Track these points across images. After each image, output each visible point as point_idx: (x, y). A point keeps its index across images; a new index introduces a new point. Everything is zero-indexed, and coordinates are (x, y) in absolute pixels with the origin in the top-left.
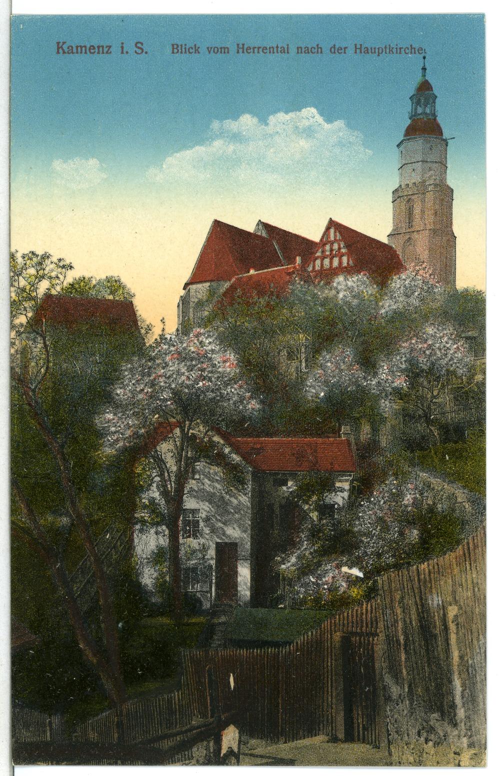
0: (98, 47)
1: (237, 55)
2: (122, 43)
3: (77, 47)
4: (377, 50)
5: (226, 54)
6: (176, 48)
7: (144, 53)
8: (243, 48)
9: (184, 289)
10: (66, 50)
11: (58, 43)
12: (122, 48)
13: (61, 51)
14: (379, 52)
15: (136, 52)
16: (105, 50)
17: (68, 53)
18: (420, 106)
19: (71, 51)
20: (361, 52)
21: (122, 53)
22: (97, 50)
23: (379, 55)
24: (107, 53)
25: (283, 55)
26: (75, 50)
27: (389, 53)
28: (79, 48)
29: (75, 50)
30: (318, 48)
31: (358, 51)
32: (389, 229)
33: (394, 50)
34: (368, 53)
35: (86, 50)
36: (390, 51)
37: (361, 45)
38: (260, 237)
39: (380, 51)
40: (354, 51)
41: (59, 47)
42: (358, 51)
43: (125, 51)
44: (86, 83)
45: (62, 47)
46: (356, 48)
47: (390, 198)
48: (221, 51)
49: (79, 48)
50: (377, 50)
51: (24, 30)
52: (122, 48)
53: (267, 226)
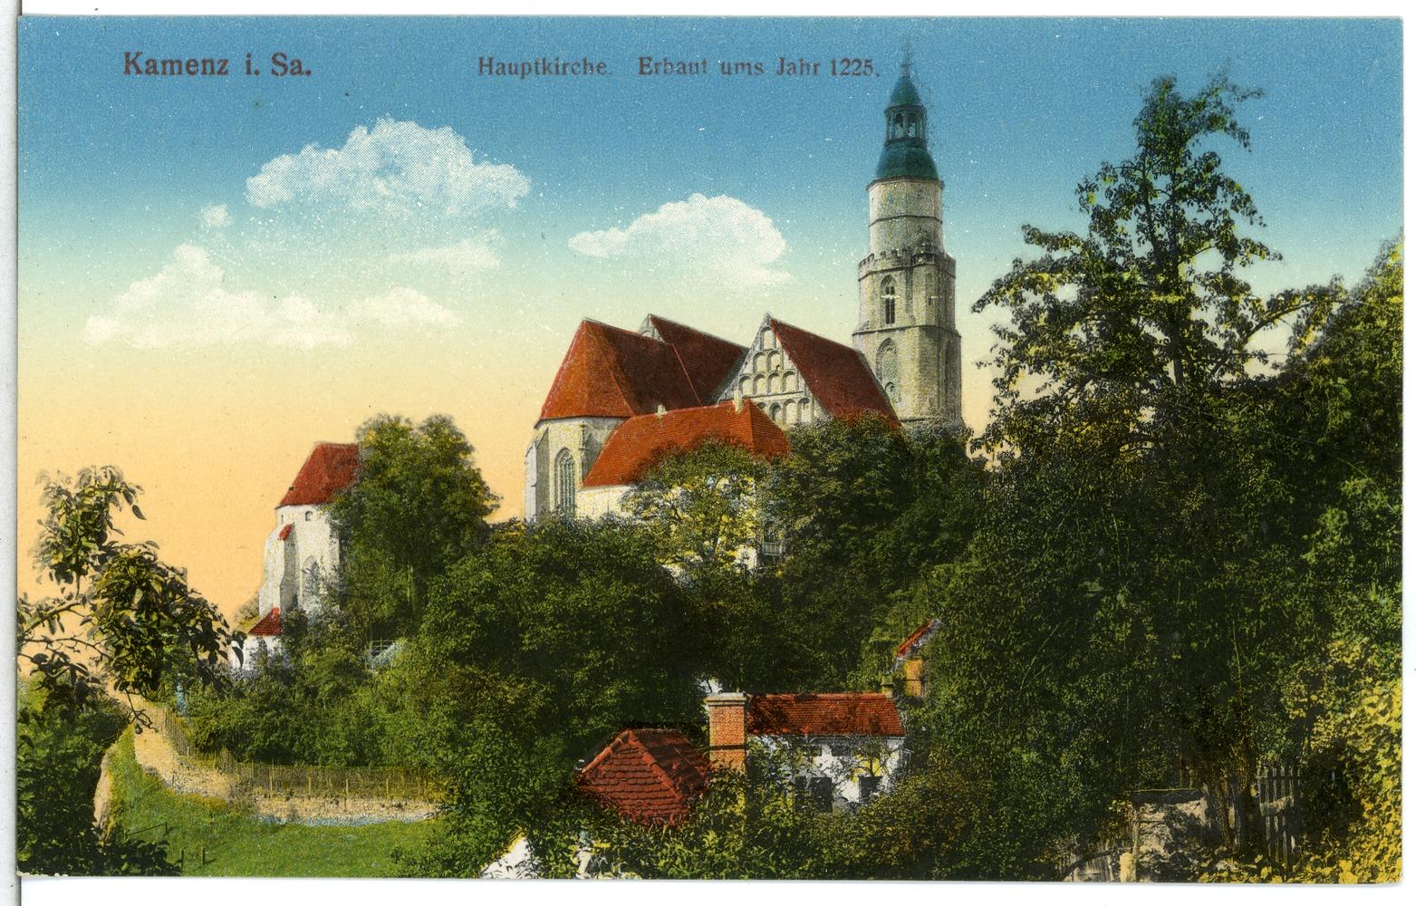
0: (204, 62)
1: (126, 77)
2: (249, 56)
3: (164, 63)
4: (520, 68)
5: (207, 76)
6: (486, 65)
7: (288, 72)
8: (490, 66)
9: (536, 427)
10: (143, 67)
11: (128, 55)
12: (248, 63)
13: (132, 68)
14: (523, 70)
15: (274, 72)
16: (217, 68)
17: (147, 72)
18: (901, 126)
19: (152, 68)
20: (491, 73)
21: (249, 72)
22: (200, 67)
23: (523, 77)
24: (220, 72)
25: (172, 77)
26: (160, 68)
27: (544, 73)
28: (168, 65)
29: (160, 68)
30: (585, 64)
31: (486, 69)
32: (855, 326)
33: (553, 68)
34: (504, 73)
35: (510, 68)
36: (544, 69)
37: (491, 59)
38: (646, 340)
39: (526, 71)
40: (124, 69)
41: (130, 62)
42: (486, 69)
43: (252, 70)
44: (158, 116)
45: (134, 62)
46: (481, 65)
47: (854, 274)
48: (205, 69)
49: (168, 65)
50: (520, 68)
51: (40, 41)
52: (248, 63)
53: (658, 323)
